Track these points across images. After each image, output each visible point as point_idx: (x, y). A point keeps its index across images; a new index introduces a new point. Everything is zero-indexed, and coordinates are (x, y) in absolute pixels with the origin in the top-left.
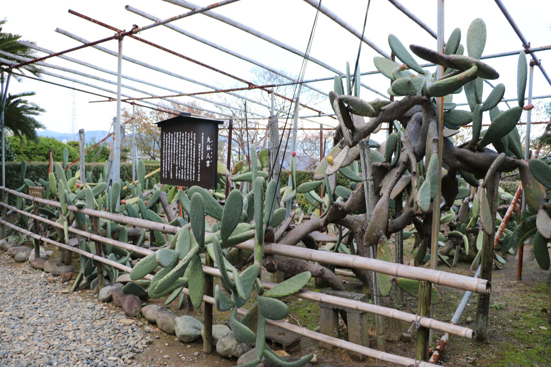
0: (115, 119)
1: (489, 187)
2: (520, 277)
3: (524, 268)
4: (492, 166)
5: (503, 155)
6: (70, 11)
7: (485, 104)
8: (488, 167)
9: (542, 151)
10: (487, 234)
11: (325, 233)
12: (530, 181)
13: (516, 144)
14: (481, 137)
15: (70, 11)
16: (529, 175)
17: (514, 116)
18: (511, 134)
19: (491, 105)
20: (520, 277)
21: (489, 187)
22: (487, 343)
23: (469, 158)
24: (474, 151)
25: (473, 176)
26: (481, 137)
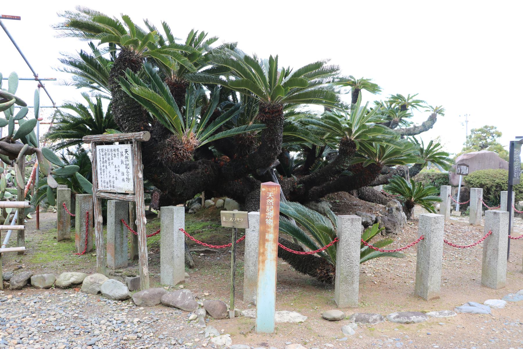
0: (493, 127)
1: (19, 164)
2: (38, 228)
3: (40, 224)
4: (21, 152)
5: (27, 145)
6: (18, 18)
7: (16, 116)
8: (18, 152)
9: (46, 144)
10: (20, 188)
11: (124, 15)
12: (43, 160)
13: (34, 139)
14: (14, 135)
15: (18, 18)
16: (42, 157)
17: (33, 123)
18: (31, 134)
19: (20, 117)
20: (38, 228)
21: (19, 164)
22: (25, 255)
23: (6, 147)
24: (9, 143)
25: (7, 157)
26: (14, 135)
